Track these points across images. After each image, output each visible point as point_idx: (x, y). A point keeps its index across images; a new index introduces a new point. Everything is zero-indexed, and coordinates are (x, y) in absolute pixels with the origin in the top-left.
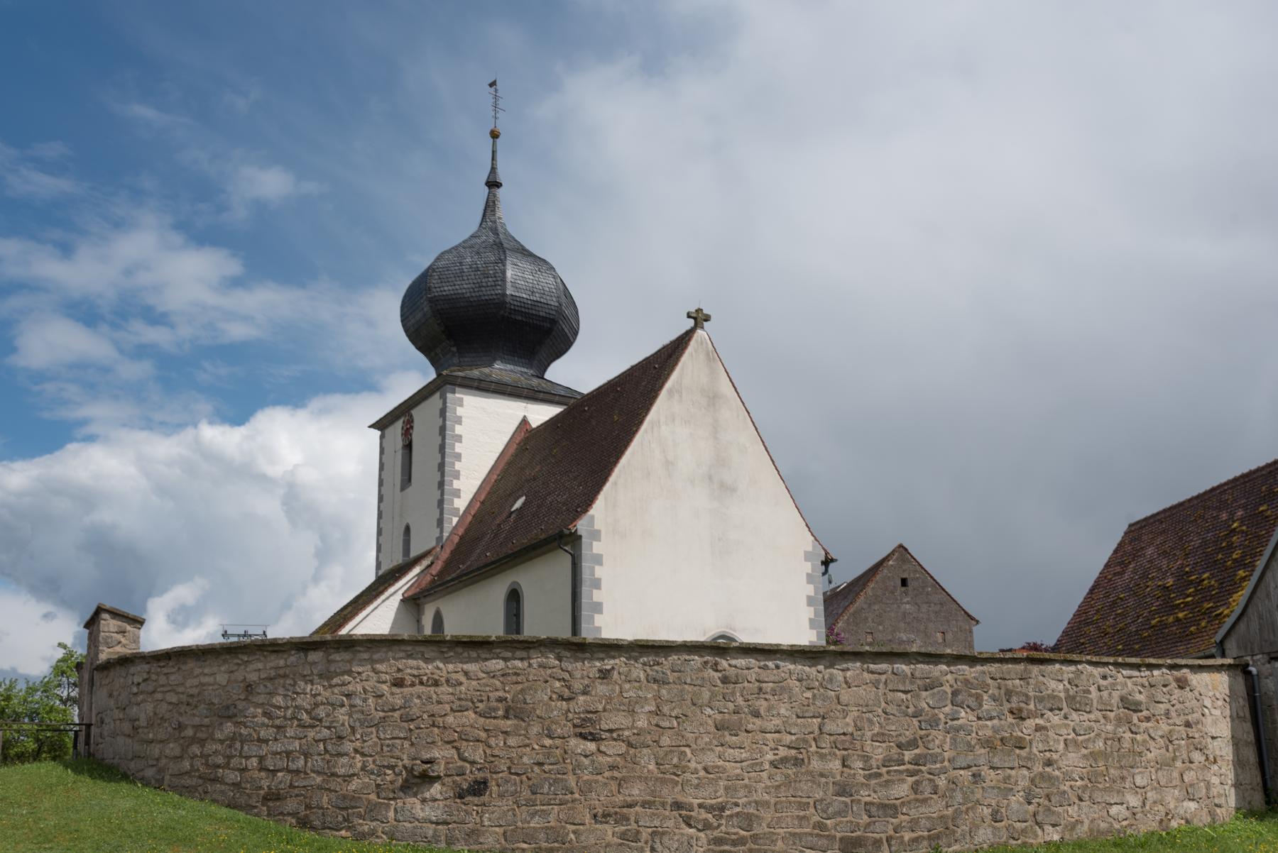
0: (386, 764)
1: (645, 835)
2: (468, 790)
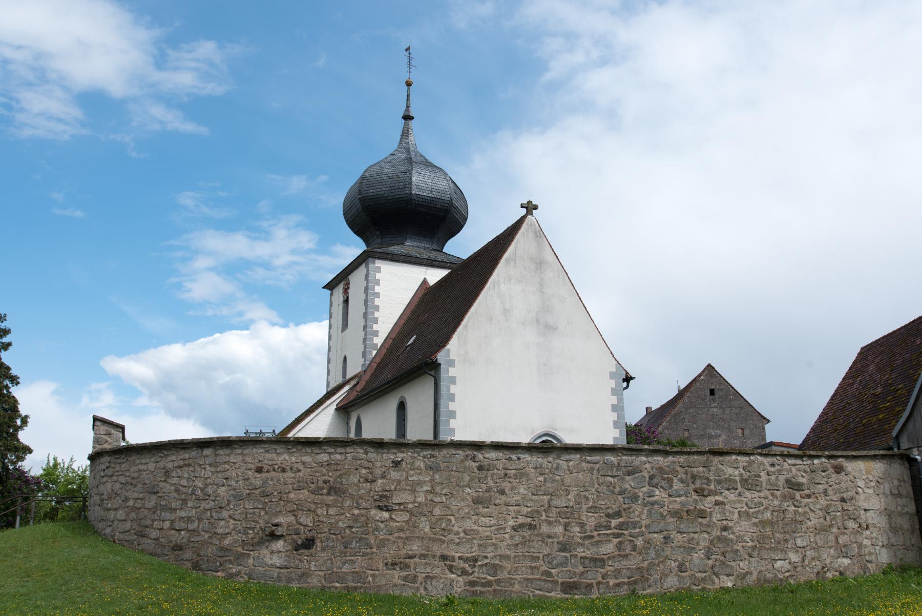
0: (249, 526)
1: (420, 579)
2: (301, 545)
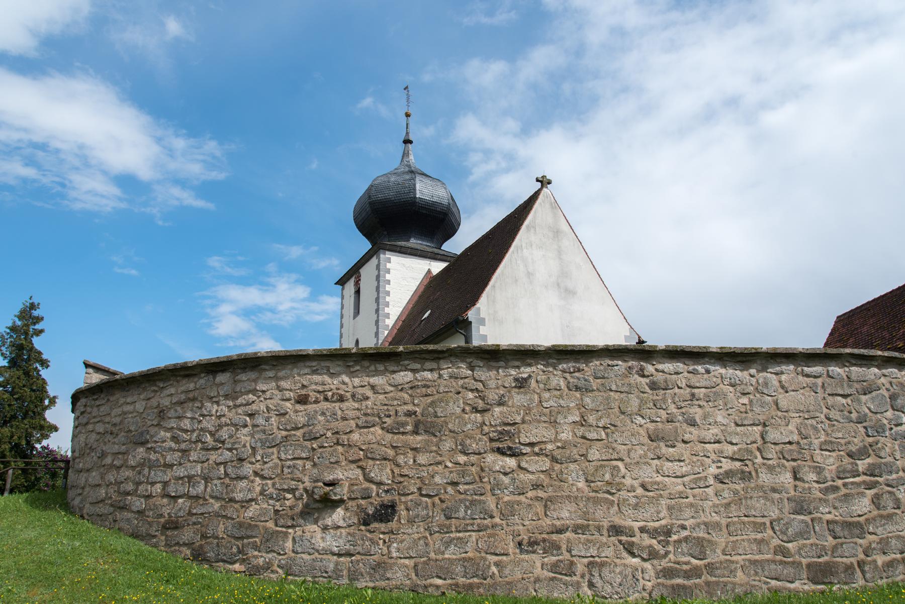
0: (286, 487)
1: (580, 568)
2: (373, 516)
